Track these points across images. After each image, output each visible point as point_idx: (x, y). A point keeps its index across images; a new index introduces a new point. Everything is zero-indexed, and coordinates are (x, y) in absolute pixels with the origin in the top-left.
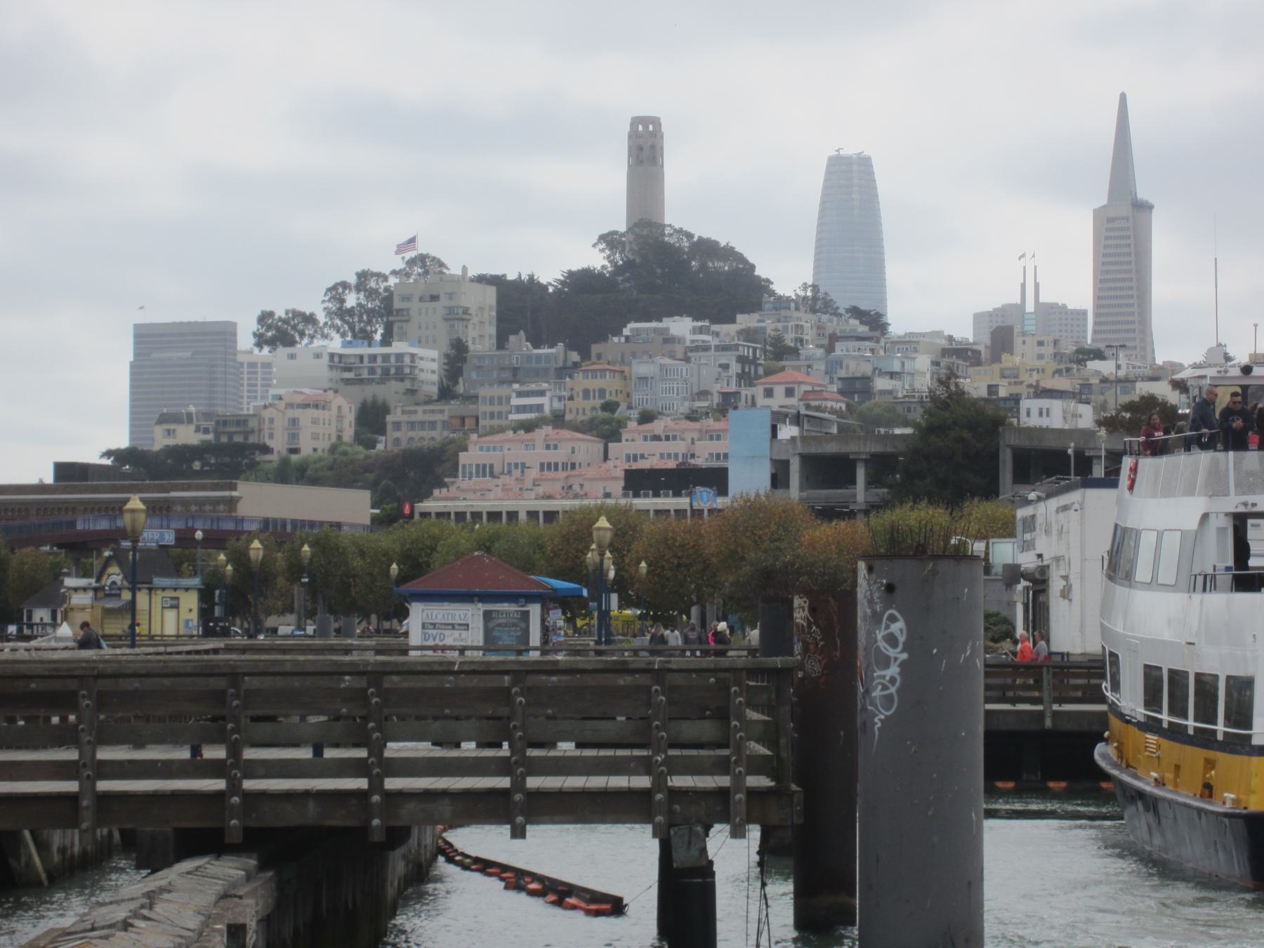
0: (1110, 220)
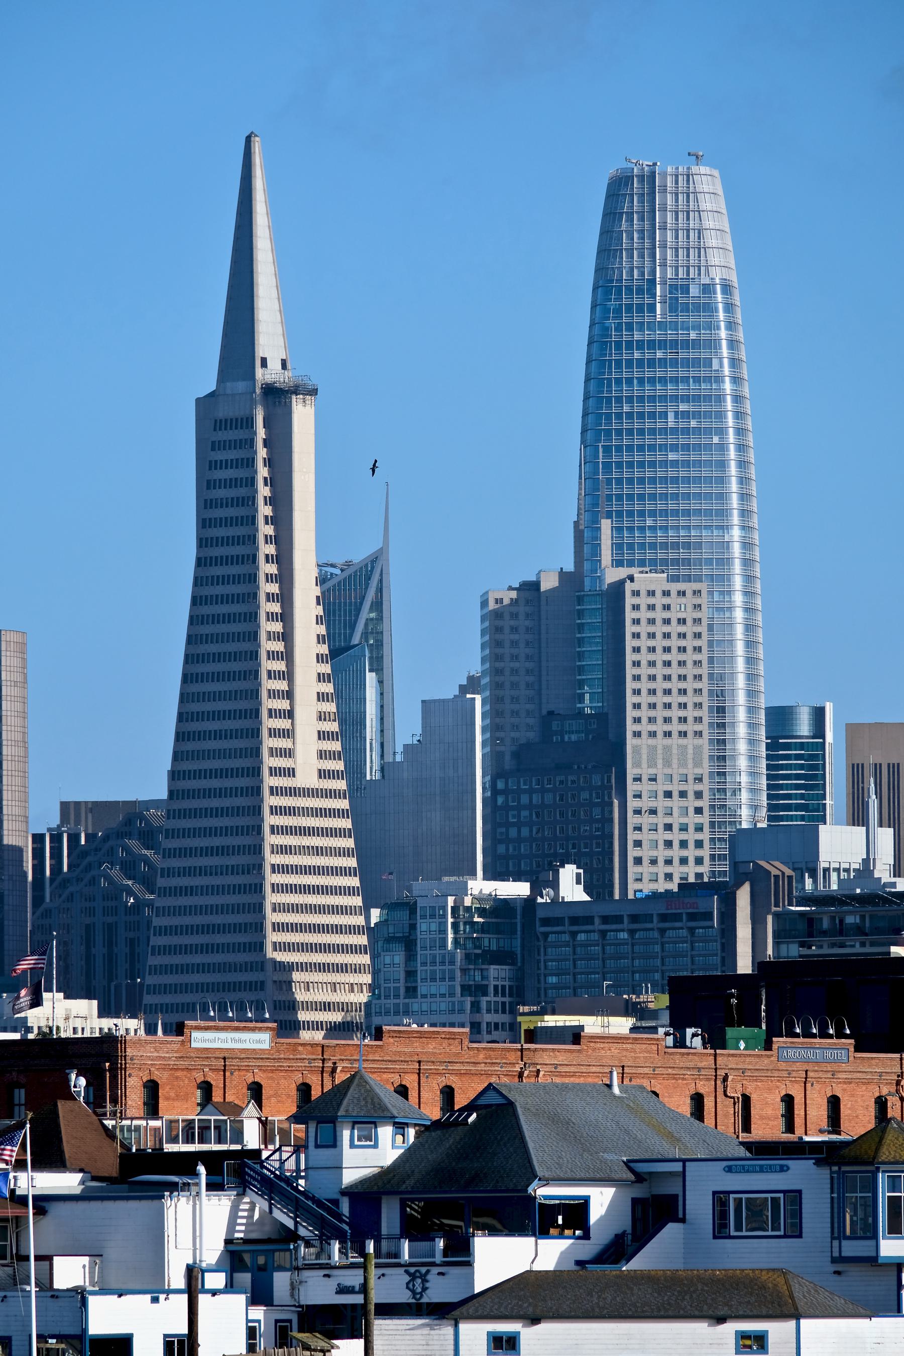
0: (221, 424)
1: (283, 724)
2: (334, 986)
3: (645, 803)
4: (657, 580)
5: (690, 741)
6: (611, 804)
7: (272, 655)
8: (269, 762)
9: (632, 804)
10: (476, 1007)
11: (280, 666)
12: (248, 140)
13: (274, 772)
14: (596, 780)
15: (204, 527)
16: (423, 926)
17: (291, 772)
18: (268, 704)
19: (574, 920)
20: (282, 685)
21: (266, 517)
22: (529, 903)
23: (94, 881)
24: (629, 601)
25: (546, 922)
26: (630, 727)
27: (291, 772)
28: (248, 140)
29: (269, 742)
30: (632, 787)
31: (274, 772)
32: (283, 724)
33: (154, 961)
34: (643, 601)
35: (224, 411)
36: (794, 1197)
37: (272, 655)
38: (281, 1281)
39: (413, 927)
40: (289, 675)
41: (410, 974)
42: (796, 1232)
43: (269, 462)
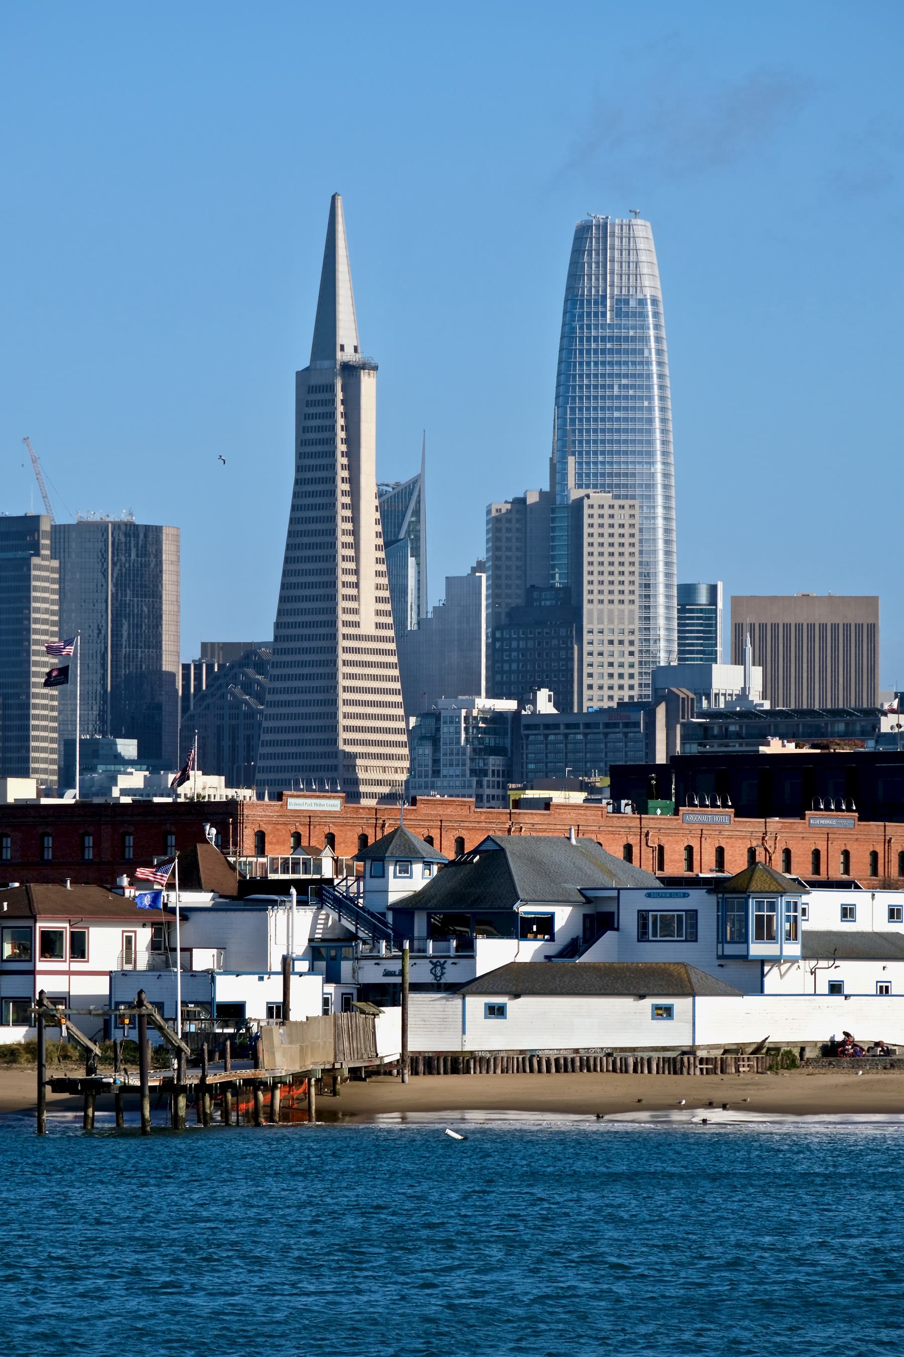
0: (312, 389)
1: (352, 592)
2: (384, 769)
3: (596, 648)
4: (605, 498)
5: (626, 607)
6: (573, 648)
7: (345, 545)
8: (342, 617)
9: (586, 648)
10: (480, 784)
11: (351, 552)
12: (334, 198)
13: (346, 624)
14: (563, 632)
15: (300, 458)
16: (444, 729)
17: (357, 624)
18: (342, 578)
19: (547, 727)
20: (352, 566)
21: (342, 452)
22: (517, 714)
23: (223, 696)
24: (586, 511)
25: (528, 727)
26: (586, 597)
27: (357, 624)
28: (334, 198)
29: (342, 604)
30: (586, 637)
31: (346, 624)
32: (352, 592)
33: (262, 750)
34: (596, 512)
35: (315, 380)
36: (693, 914)
37: (345, 545)
38: (346, 967)
39: (438, 729)
40: (356, 559)
41: (436, 761)
42: (693, 937)
43: (345, 415)
